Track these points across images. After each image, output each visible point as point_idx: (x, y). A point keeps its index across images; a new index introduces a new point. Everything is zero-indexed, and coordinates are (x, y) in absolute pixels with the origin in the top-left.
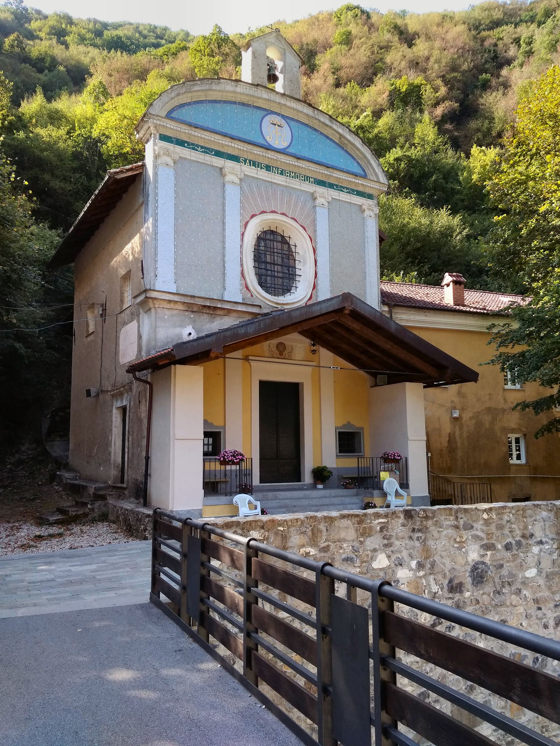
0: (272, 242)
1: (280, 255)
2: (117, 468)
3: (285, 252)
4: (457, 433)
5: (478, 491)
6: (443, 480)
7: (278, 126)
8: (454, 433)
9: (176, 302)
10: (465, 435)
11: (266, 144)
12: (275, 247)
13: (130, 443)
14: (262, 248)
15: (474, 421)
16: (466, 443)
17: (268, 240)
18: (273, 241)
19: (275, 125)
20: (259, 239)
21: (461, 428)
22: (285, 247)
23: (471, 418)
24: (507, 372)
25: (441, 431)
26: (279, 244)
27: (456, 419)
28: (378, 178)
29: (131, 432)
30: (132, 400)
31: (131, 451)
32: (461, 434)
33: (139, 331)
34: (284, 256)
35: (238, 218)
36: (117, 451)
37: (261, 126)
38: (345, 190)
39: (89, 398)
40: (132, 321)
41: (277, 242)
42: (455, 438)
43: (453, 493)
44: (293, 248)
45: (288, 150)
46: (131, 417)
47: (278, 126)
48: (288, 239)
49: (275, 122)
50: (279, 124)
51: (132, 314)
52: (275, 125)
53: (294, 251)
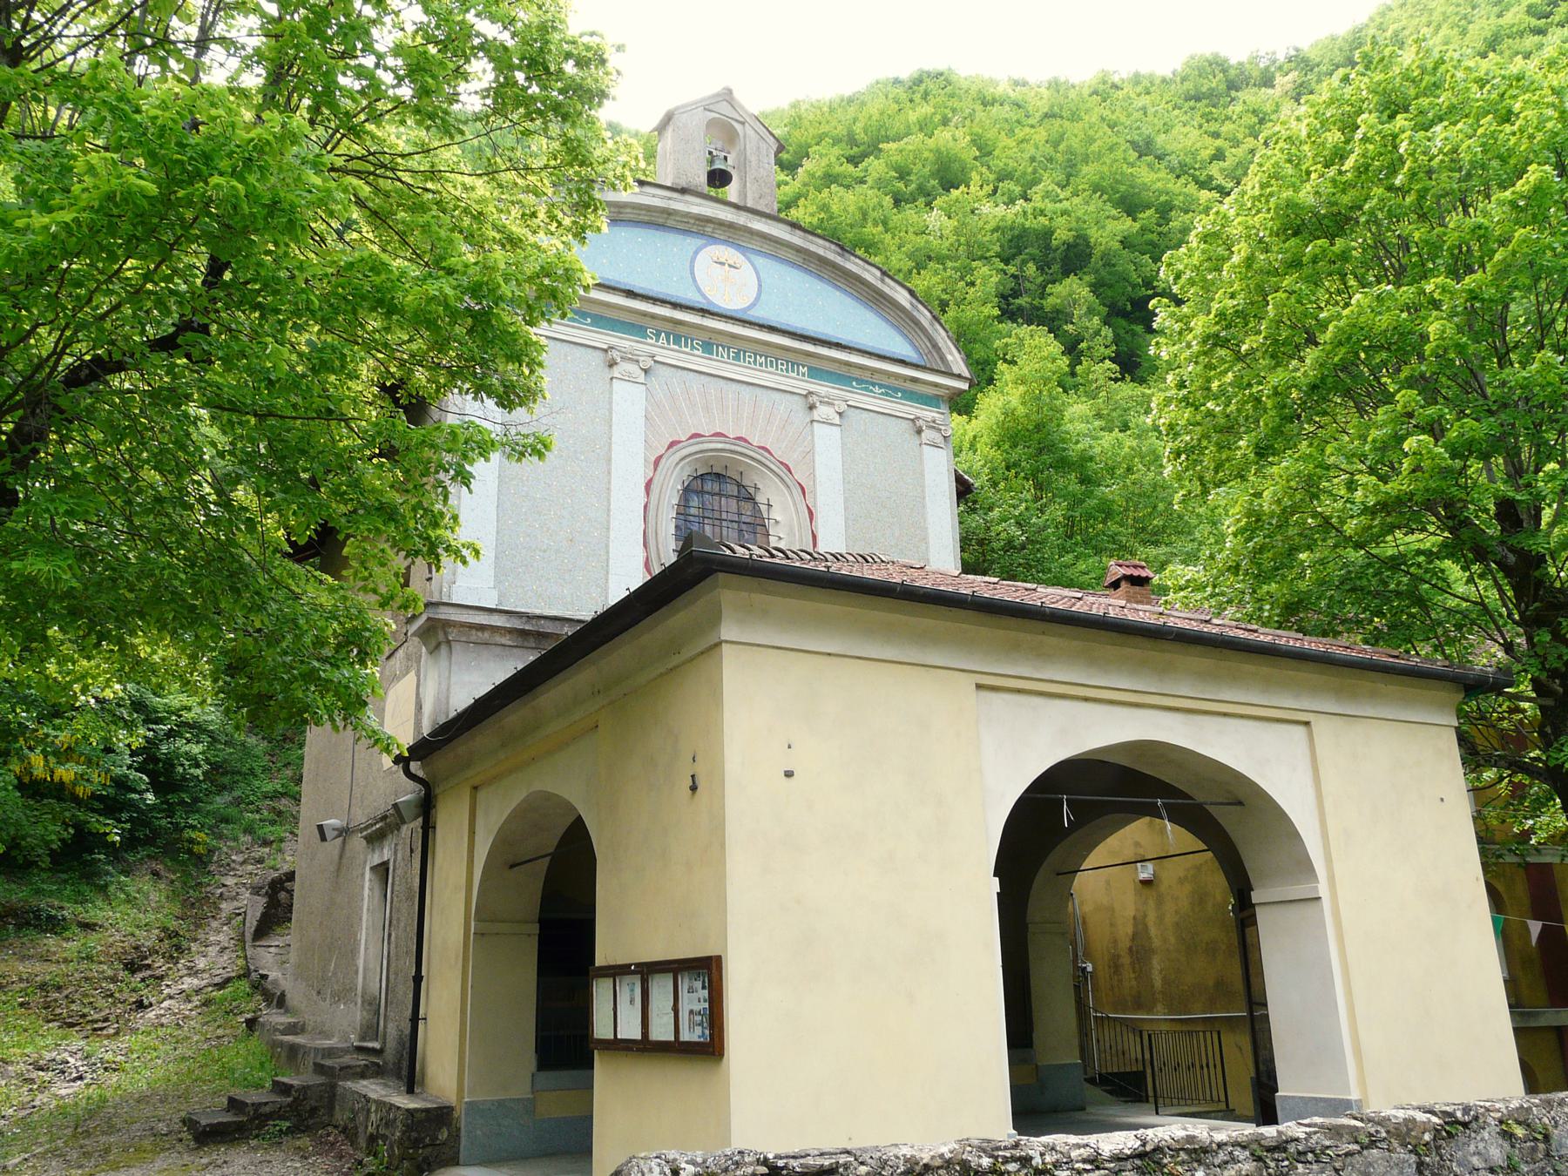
0: (717, 498)
1: (735, 526)
2: (370, 1004)
3: (744, 519)
4: (1152, 917)
5: (1210, 1048)
6: (1124, 1028)
7: (730, 266)
8: (1145, 916)
9: (494, 629)
10: (1170, 919)
11: (700, 299)
12: (724, 509)
13: (393, 946)
14: (693, 511)
15: (1188, 888)
16: (1172, 940)
17: (708, 493)
18: (720, 495)
19: (722, 264)
20: (687, 491)
21: (1160, 902)
22: (747, 508)
23: (1181, 881)
24: (157, 910)
25: (1113, 910)
26: (733, 502)
27: (1146, 883)
28: (943, 359)
29: (394, 922)
30: (399, 847)
31: (393, 965)
32: (1161, 918)
33: (418, 694)
34: (744, 527)
35: (640, 448)
36: (371, 966)
37: (692, 273)
38: (877, 389)
39: (325, 844)
40: (407, 673)
41: (727, 497)
42: (1146, 927)
43: (1140, 1057)
44: (763, 508)
45: (751, 312)
46: (396, 888)
47: (730, 266)
48: (752, 491)
49: (723, 260)
50: (731, 262)
51: (408, 657)
52: (722, 264)
53: (765, 516)
